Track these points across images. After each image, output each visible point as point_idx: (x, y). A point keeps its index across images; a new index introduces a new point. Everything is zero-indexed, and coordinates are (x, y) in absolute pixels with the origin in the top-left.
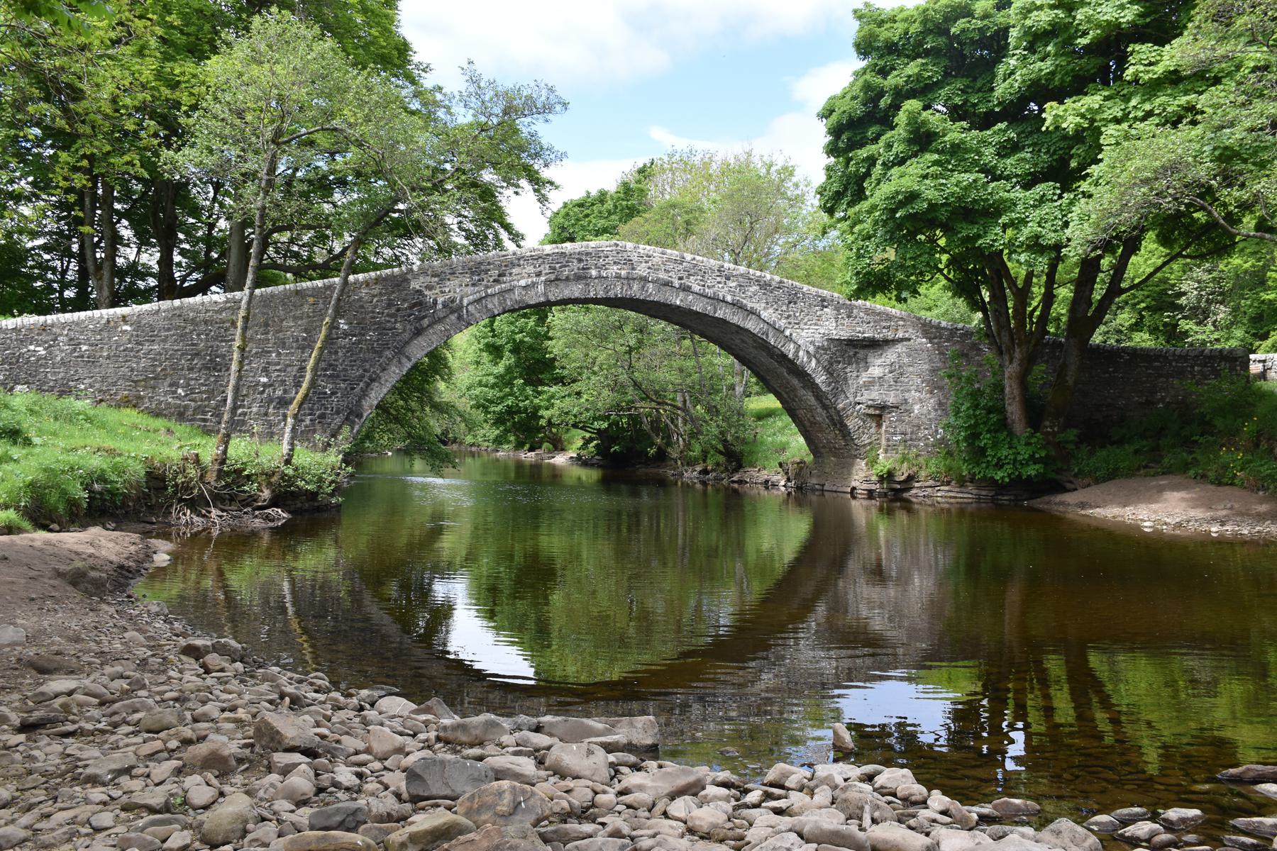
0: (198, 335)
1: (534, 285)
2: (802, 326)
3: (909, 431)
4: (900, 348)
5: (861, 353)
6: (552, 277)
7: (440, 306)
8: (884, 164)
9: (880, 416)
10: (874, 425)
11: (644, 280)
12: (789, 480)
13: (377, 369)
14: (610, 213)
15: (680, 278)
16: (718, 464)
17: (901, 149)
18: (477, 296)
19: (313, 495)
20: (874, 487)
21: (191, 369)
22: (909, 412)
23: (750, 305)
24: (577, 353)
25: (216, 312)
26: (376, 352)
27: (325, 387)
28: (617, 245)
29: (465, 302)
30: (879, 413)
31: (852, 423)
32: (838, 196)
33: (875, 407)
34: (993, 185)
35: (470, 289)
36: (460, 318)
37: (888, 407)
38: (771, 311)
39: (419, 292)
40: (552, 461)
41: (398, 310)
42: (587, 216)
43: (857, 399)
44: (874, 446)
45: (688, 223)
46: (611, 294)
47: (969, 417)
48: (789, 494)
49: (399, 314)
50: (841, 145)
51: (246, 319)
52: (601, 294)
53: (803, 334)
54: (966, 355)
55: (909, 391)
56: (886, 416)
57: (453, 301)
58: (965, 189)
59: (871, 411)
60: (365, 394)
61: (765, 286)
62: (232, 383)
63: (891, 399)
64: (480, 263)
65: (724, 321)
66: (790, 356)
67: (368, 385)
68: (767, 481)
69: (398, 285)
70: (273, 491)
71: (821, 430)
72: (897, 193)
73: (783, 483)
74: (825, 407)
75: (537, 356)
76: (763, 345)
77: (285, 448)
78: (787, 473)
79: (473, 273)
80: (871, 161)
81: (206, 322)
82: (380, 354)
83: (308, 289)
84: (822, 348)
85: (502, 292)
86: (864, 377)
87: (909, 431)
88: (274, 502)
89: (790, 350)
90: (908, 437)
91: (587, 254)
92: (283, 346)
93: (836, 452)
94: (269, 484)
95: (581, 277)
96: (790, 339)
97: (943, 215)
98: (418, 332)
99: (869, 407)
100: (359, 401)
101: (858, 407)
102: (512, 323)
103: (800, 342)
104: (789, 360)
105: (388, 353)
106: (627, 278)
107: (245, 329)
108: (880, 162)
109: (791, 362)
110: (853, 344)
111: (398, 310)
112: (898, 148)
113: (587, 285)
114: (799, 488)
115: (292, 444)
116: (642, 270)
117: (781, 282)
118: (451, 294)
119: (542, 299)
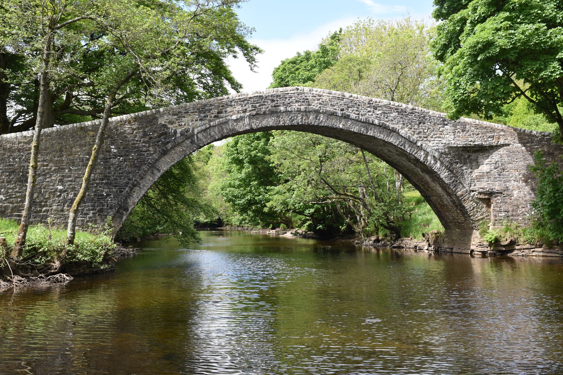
0: (14, 159)
1: (242, 119)
2: (429, 138)
3: (510, 209)
4: (502, 151)
5: (473, 156)
6: (254, 113)
7: (178, 135)
8: (471, 22)
9: (489, 200)
10: (485, 206)
11: (317, 112)
12: (429, 245)
13: (137, 178)
14: (313, 67)
15: (342, 110)
16: (386, 235)
17: (482, 11)
18: (203, 128)
19: (89, 264)
20: (486, 249)
21: (9, 182)
22: (510, 196)
23: (391, 126)
24: (287, 163)
25: (26, 143)
26: (136, 167)
27: (102, 191)
28: (298, 89)
29: (196, 131)
30: (487, 198)
31: (468, 205)
32: (445, 47)
33: (485, 194)
34: (550, 31)
35: (199, 123)
36: (192, 142)
37: (495, 193)
38: (406, 129)
39: (165, 126)
40: (285, 236)
41: (151, 138)
42: (298, 69)
43: (471, 188)
44: (484, 221)
45: (360, 71)
46: (295, 123)
47: (550, 198)
48: (430, 255)
49: (151, 141)
50: (444, 11)
51: (37, 147)
52: (288, 123)
53: (431, 144)
54: (552, 154)
55: (509, 181)
56: (494, 200)
57: (187, 131)
58: (531, 35)
59: (482, 196)
60: (129, 195)
61: (402, 112)
62: (29, 190)
63: (497, 187)
64: (205, 105)
65: (374, 138)
66: (422, 159)
67: (131, 189)
68: (416, 247)
69: (150, 122)
70: (61, 262)
71: (448, 211)
72: (478, 43)
73: (426, 247)
74: (449, 194)
75: (266, 165)
76: (403, 153)
77: (69, 232)
78: (428, 241)
79: (200, 112)
80: (463, 21)
81: (19, 150)
82: (139, 168)
83: (89, 126)
84: (445, 153)
85: (220, 124)
86: (476, 173)
87: (510, 209)
88: (62, 270)
89: (421, 156)
90: (510, 214)
91: (277, 96)
92: (73, 164)
93: (459, 225)
94: (59, 258)
95: (274, 112)
96: (420, 148)
97: (512, 57)
98: (165, 153)
99: (480, 193)
100: (126, 199)
101: (472, 194)
102: (248, 144)
103: (428, 150)
104: (421, 162)
105: (145, 167)
106: (305, 111)
107: (36, 154)
108: (469, 21)
109: (423, 164)
110: (466, 149)
111: (151, 138)
112: (481, 10)
113: (278, 117)
114: (437, 251)
115: (73, 230)
116: (315, 105)
117: (413, 109)
118: (186, 127)
119: (248, 128)
